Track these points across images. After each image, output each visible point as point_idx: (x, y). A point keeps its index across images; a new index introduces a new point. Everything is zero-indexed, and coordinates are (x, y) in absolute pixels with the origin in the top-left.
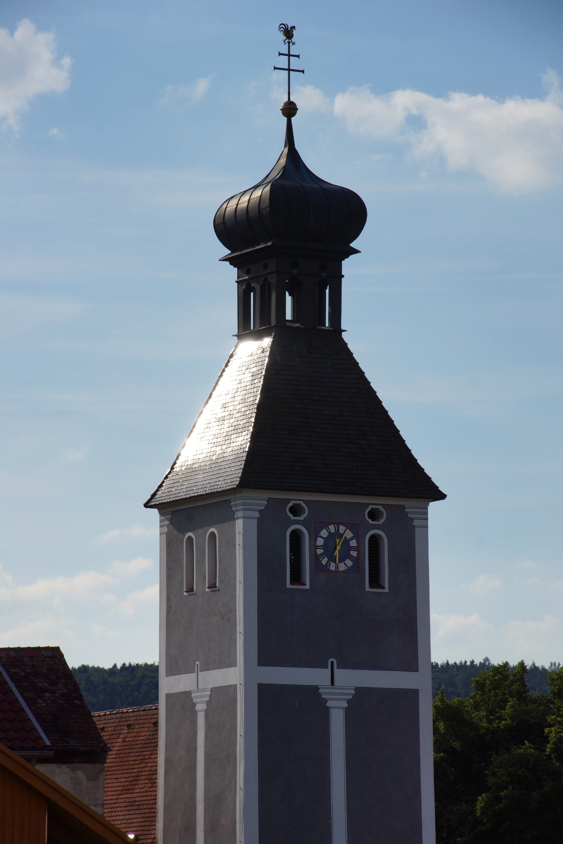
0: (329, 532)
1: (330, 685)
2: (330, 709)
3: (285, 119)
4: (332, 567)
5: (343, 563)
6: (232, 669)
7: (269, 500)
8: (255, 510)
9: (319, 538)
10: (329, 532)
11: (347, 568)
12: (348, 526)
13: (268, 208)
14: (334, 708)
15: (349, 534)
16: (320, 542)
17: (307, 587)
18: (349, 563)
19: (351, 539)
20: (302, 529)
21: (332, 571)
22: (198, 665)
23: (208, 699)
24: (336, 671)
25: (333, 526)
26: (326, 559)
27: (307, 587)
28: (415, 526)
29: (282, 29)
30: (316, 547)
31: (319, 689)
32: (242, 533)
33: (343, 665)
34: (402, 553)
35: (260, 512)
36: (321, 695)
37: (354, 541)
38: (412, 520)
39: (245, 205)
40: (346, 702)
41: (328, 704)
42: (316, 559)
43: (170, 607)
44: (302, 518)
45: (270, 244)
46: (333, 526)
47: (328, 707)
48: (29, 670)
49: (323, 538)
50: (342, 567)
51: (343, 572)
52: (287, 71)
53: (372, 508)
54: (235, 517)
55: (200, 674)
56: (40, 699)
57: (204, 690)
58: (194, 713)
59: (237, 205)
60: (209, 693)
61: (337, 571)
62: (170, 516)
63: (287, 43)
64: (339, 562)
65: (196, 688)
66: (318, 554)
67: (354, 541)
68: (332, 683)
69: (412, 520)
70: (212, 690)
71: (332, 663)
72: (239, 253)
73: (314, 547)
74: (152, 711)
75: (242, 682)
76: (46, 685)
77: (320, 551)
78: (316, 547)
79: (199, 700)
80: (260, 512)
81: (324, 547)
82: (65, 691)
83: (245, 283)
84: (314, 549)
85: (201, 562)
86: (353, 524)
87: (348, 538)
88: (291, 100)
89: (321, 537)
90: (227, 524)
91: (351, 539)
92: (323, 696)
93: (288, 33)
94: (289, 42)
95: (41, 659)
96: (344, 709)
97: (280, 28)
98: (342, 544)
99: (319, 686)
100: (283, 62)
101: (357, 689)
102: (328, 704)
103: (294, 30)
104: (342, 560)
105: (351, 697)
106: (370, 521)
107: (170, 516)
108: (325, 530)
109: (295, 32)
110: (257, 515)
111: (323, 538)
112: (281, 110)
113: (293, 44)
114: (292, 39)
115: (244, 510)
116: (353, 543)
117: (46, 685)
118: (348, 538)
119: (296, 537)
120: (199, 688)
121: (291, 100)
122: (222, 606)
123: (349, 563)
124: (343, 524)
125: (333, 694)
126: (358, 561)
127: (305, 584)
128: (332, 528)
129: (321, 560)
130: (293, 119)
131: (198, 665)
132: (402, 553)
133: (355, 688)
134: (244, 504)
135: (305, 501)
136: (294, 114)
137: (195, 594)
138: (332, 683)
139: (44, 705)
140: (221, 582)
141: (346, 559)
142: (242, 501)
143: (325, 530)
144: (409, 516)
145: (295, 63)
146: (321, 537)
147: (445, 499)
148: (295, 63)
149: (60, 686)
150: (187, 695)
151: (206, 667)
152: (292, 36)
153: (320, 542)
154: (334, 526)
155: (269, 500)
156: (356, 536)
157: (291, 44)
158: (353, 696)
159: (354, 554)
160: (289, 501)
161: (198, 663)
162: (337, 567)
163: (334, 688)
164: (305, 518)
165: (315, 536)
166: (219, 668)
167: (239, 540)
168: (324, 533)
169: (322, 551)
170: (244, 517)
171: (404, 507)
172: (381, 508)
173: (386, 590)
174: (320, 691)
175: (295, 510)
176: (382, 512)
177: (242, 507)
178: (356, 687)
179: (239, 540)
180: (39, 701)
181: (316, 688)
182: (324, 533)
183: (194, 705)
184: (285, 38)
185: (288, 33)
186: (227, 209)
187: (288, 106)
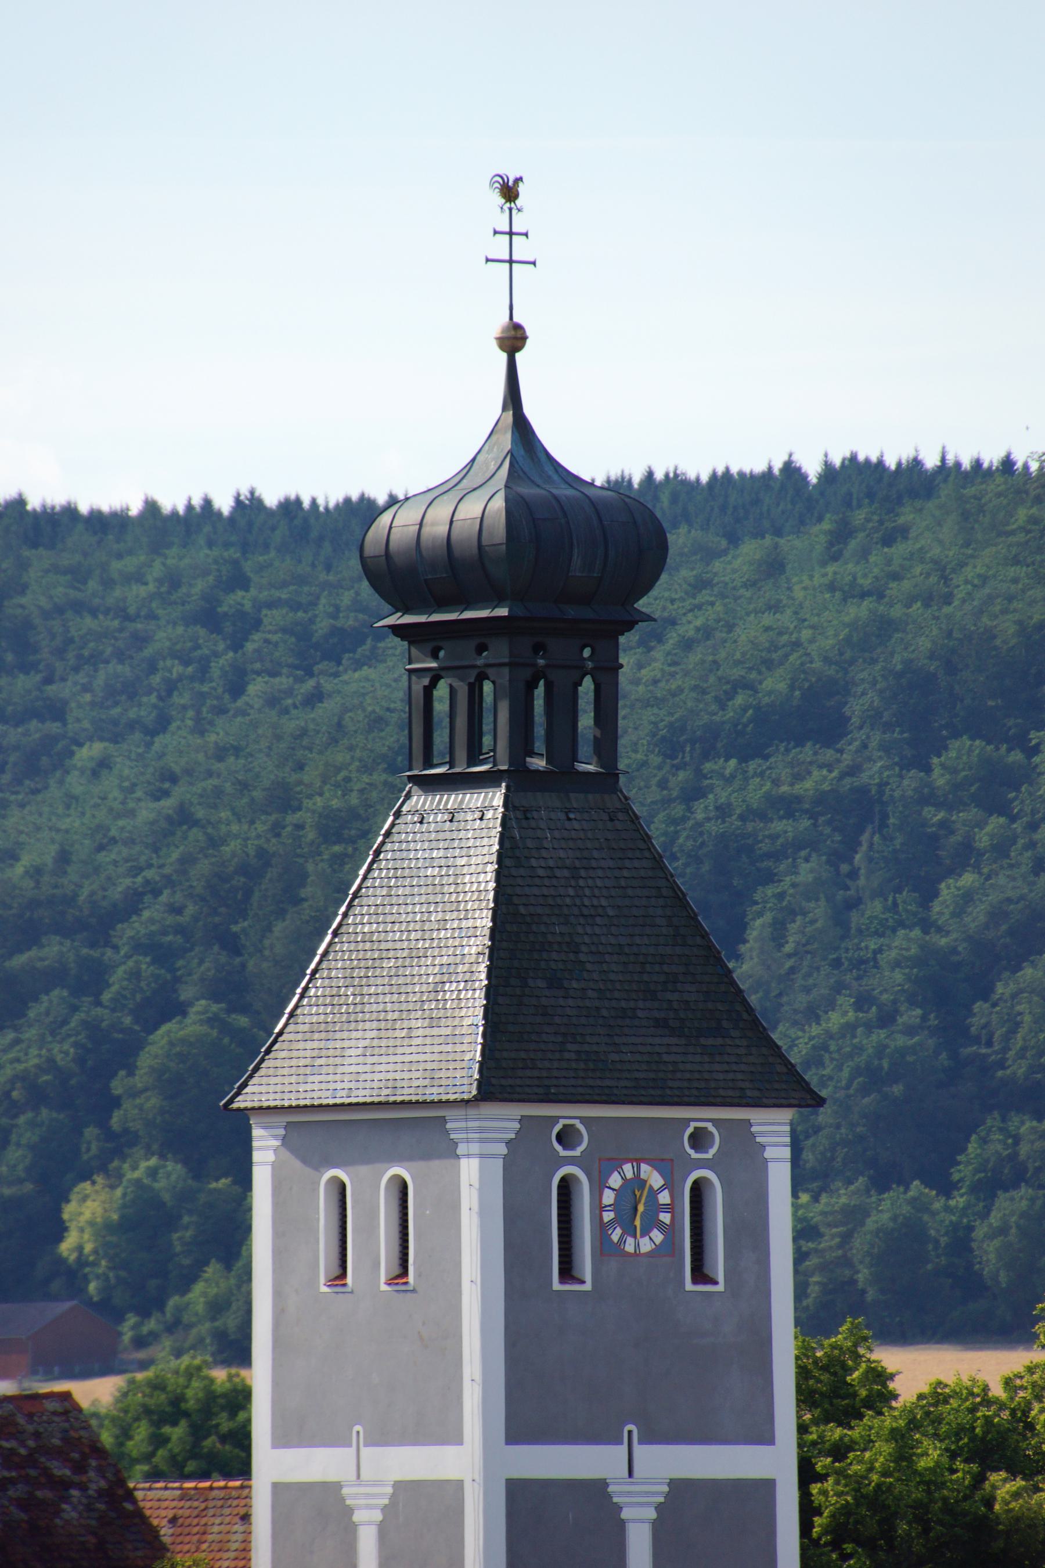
3: (504, 356)
4: (629, 1247)
6: (450, 1450)
7: (522, 1119)
9: (606, 1190)
10: (624, 1178)
12: (656, 1163)
13: (504, 547)
14: (634, 1521)
15: (656, 1180)
16: (608, 1197)
17: (588, 1287)
18: (657, 1236)
19: (661, 1189)
21: (629, 1254)
22: (358, 1432)
23: (386, 1501)
24: (638, 1449)
25: (630, 1165)
26: (618, 1232)
27: (588, 1287)
29: (497, 185)
30: (602, 1209)
32: (476, 1185)
33: (650, 1437)
35: (509, 1143)
37: (666, 1193)
38: (763, 1147)
39: (443, 529)
40: (653, 1509)
42: (601, 1229)
43: (283, 1311)
44: (577, 1152)
45: (503, 612)
46: (630, 1165)
48: (31, 1443)
49: (613, 1190)
50: (646, 1246)
51: (649, 1254)
52: (507, 265)
53: (696, 1128)
54: (459, 1152)
55: (365, 1451)
56: (66, 1503)
57: (376, 1483)
58: (350, 1531)
59: (421, 524)
60: (389, 1490)
61: (636, 1254)
62: (282, 1132)
63: (507, 211)
64: (642, 1236)
65: (354, 1478)
67: (666, 1193)
68: (631, 1474)
69: (763, 1147)
70: (398, 1485)
71: (630, 1432)
72: (422, 619)
73: (599, 1208)
74: (155, 1492)
75: (476, 1477)
76: (68, 1472)
77: (608, 1216)
78: (602, 1209)
79: (362, 1502)
80: (509, 1143)
81: (615, 1207)
82: (103, 1484)
83: (430, 674)
84: (598, 1212)
85: (369, 1230)
87: (656, 1188)
88: (516, 319)
89: (610, 1188)
90: (436, 1164)
91: (661, 1189)
92: (615, 1500)
93: (509, 192)
94: (510, 209)
95: (45, 1418)
97: (492, 184)
100: (500, 247)
101: (673, 1483)
103: (520, 184)
104: (645, 1232)
105: (662, 1500)
106: (691, 1152)
107: (282, 1132)
108: (616, 1174)
109: (522, 188)
110: (503, 1149)
111: (613, 1190)
112: (497, 339)
113: (519, 210)
114: (517, 202)
115: (482, 1141)
116: (664, 1198)
117: (68, 1472)
118: (656, 1188)
119: (566, 1187)
120: (362, 1477)
121: (516, 319)
122: (424, 1324)
123: (657, 1236)
125: (629, 1494)
126: (671, 1232)
127: (583, 1282)
128: (628, 1169)
130: (518, 356)
131: (358, 1432)
134: (481, 1130)
135: (582, 1119)
136: (519, 349)
137: (352, 1292)
138: (631, 1474)
139: (74, 1515)
140: (420, 1276)
141: (651, 1230)
142: (476, 1124)
143: (616, 1174)
144: (758, 1139)
145: (522, 249)
146: (610, 1188)
148: (522, 249)
149: (92, 1474)
150: (331, 1490)
151: (381, 1437)
152: (517, 196)
153: (608, 1197)
155: (522, 1119)
156: (670, 1185)
157: (514, 212)
159: (665, 1218)
160: (556, 1119)
161: (358, 1428)
162: (637, 1246)
163: (633, 1483)
165: (599, 1185)
166: (415, 1443)
167: (469, 1200)
168: (615, 1181)
170: (482, 1156)
171: (748, 1123)
172: (710, 1126)
173: (720, 1288)
174: (611, 1489)
175: (566, 1138)
176: (711, 1133)
177: (477, 1135)
179: (469, 1200)
180: (64, 1506)
181: (603, 1484)
182: (615, 1181)
183: (349, 1511)
184: (503, 201)
185: (509, 192)
186: (393, 530)
187: (513, 333)
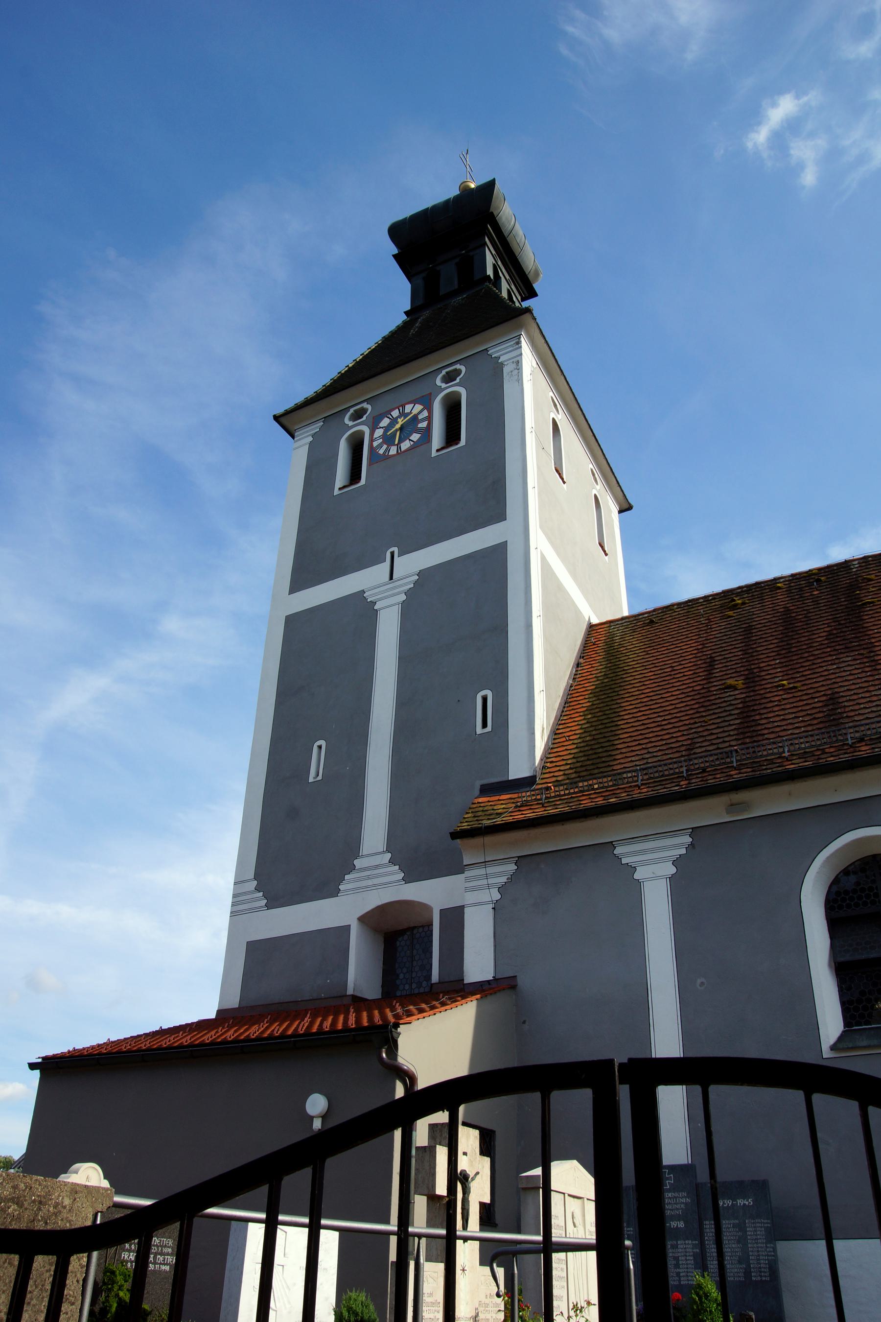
11: (412, 443)
31: (615, 847)
96: (668, 879)
105: (683, 851)
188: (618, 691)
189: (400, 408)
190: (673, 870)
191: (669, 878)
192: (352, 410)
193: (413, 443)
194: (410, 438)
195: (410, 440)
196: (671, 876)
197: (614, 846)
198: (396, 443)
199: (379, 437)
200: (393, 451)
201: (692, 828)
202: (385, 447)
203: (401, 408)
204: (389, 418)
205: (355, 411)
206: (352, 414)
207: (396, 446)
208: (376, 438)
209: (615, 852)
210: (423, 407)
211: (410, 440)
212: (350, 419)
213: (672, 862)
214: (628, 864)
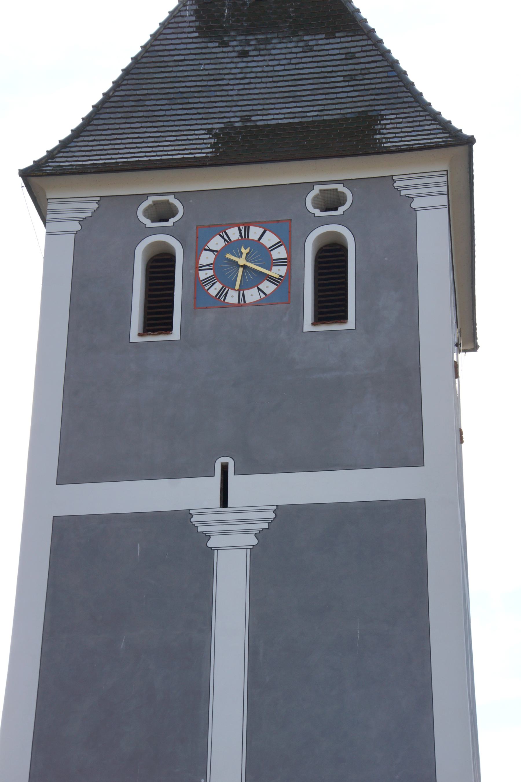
0: (227, 240)
1: (219, 506)
2: (216, 551)
5: (256, 288)
8: (82, 219)
11: (263, 296)
16: (207, 258)
19: (275, 246)
20: (330, 230)
28: (416, 209)
30: (199, 268)
31: (193, 515)
34: (386, 259)
35: (81, 221)
36: (197, 526)
37: (282, 249)
41: (211, 544)
47: (211, 548)
66: (202, 278)
67: (282, 249)
68: (224, 502)
78: (199, 268)
84: (192, 271)
86: (278, 221)
92: (200, 529)
96: (249, 550)
98: (235, 256)
99: (191, 512)
101: (278, 510)
102: (211, 544)
105: (266, 526)
124: (256, 224)
129: (207, 288)
132: (386, 259)
133: (275, 507)
138: (224, 502)
147: (475, 142)
153: (207, 258)
154: (239, 228)
158: (269, 523)
162: (241, 297)
163: (225, 512)
164: (344, 211)
169: (211, 273)
178: (277, 506)
188: (270, 49)
189: (241, 227)
190: (255, 542)
191: (250, 548)
192: (150, 201)
193: (264, 296)
194: (260, 286)
195: (259, 289)
196: (252, 547)
197: (191, 515)
198: (237, 287)
199: (208, 265)
200: (232, 297)
201: (100, 197)
202: (218, 286)
203: (242, 228)
204: (223, 237)
205: (155, 203)
206: (150, 207)
207: (238, 292)
208: (203, 266)
209: (192, 520)
210: (278, 240)
211: (259, 289)
212: (147, 213)
213: (254, 534)
214: (203, 532)
